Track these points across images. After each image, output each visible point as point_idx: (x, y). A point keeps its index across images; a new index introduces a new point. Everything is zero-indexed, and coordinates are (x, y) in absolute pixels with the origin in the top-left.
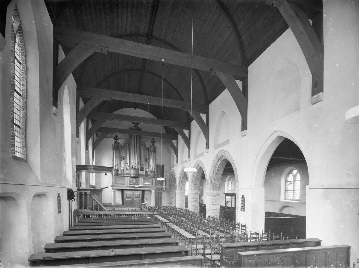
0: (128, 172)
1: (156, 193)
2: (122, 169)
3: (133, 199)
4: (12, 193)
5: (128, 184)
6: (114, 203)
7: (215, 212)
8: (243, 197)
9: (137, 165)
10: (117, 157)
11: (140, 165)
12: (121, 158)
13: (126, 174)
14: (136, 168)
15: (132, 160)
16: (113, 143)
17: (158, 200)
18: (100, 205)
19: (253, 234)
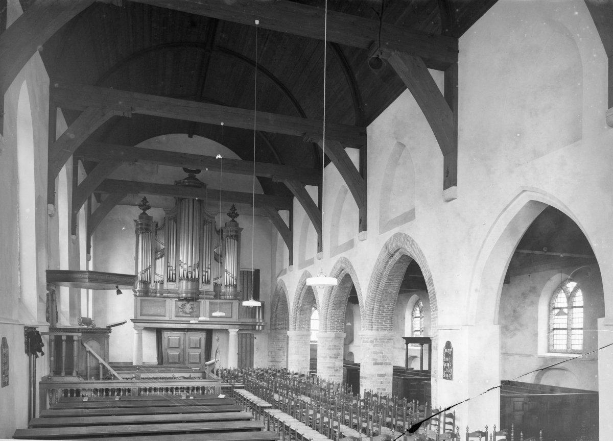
0: (171, 286)
1: (241, 336)
2: (158, 278)
3: (184, 350)
6: (138, 360)
7: (382, 383)
8: (448, 345)
9: (195, 270)
10: (145, 251)
12: (156, 252)
14: (192, 277)
16: (137, 218)
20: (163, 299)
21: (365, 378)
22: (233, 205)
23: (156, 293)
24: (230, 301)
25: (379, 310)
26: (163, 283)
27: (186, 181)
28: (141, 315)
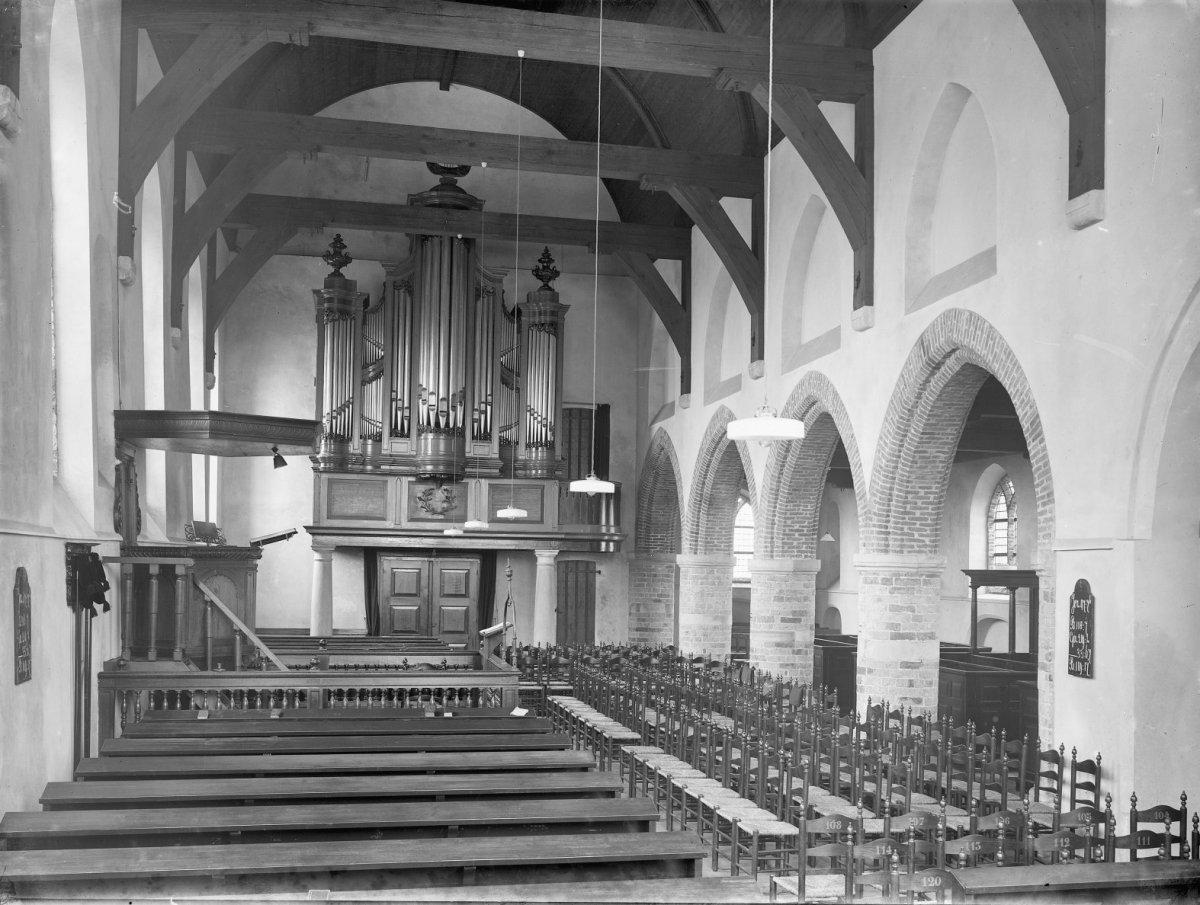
0: (401, 447)
1: (562, 567)
3: (429, 601)
7: (911, 684)
8: (1082, 590)
9: (454, 408)
10: (339, 364)
12: (365, 366)
14: (447, 424)
15: (427, 378)
16: (320, 286)
18: (244, 637)
21: (870, 671)
23: (364, 463)
26: (380, 440)
27: (434, 193)
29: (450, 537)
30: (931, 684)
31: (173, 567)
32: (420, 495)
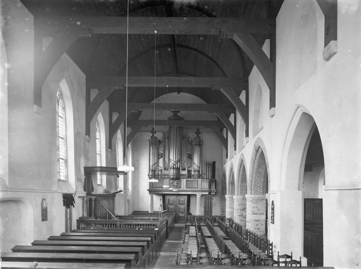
0: (166, 172)
2: (160, 168)
3: (176, 206)
4: (22, 198)
5: (185, 187)
6: (151, 211)
7: (257, 225)
8: (273, 202)
9: (177, 164)
11: (181, 164)
12: (159, 155)
13: (165, 176)
15: (171, 157)
16: (150, 138)
17: (208, 208)
18: (109, 213)
19: (282, 257)
20: (163, 179)
21: (248, 222)
22: (198, 128)
23: (159, 176)
24: (197, 179)
25: (255, 183)
26: (162, 171)
28: (152, 187)
29: (174, 191)
30: (262, 225)
31: (92, 198)
32: (171, 182)
